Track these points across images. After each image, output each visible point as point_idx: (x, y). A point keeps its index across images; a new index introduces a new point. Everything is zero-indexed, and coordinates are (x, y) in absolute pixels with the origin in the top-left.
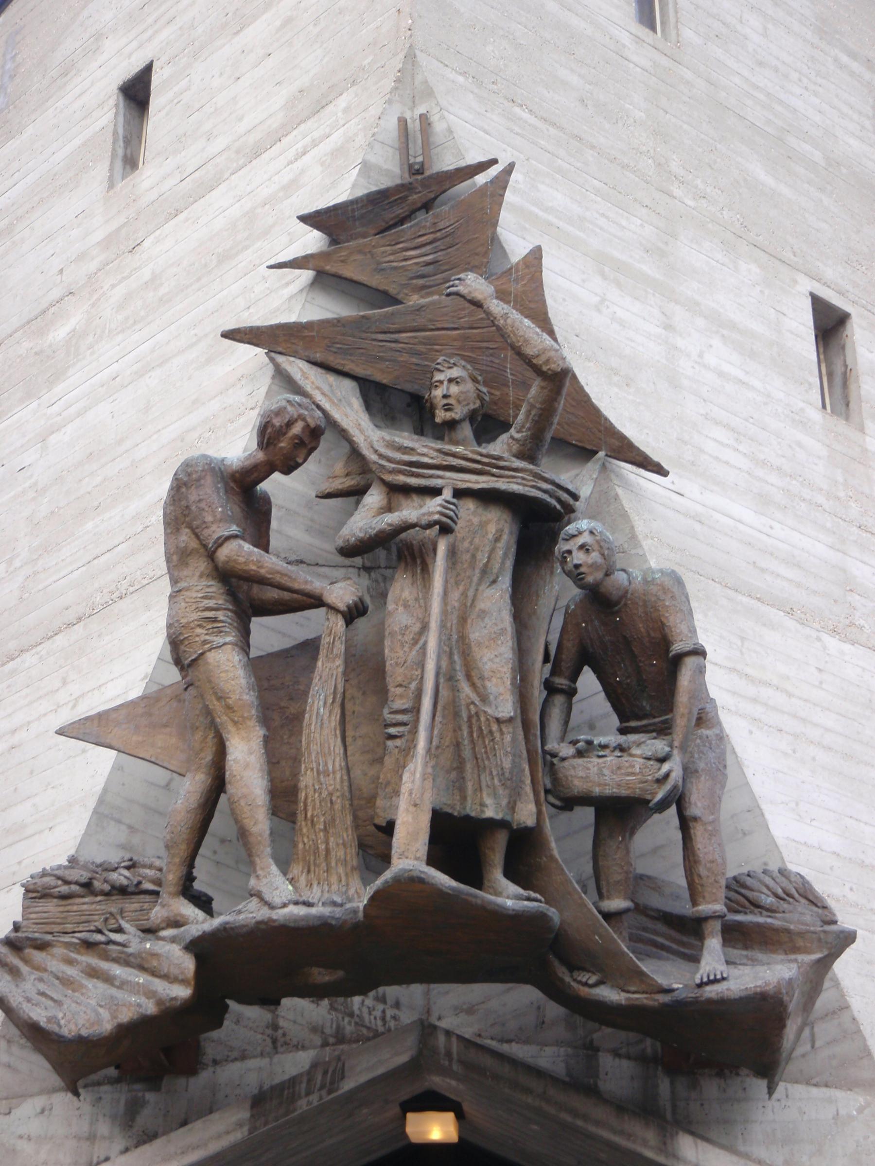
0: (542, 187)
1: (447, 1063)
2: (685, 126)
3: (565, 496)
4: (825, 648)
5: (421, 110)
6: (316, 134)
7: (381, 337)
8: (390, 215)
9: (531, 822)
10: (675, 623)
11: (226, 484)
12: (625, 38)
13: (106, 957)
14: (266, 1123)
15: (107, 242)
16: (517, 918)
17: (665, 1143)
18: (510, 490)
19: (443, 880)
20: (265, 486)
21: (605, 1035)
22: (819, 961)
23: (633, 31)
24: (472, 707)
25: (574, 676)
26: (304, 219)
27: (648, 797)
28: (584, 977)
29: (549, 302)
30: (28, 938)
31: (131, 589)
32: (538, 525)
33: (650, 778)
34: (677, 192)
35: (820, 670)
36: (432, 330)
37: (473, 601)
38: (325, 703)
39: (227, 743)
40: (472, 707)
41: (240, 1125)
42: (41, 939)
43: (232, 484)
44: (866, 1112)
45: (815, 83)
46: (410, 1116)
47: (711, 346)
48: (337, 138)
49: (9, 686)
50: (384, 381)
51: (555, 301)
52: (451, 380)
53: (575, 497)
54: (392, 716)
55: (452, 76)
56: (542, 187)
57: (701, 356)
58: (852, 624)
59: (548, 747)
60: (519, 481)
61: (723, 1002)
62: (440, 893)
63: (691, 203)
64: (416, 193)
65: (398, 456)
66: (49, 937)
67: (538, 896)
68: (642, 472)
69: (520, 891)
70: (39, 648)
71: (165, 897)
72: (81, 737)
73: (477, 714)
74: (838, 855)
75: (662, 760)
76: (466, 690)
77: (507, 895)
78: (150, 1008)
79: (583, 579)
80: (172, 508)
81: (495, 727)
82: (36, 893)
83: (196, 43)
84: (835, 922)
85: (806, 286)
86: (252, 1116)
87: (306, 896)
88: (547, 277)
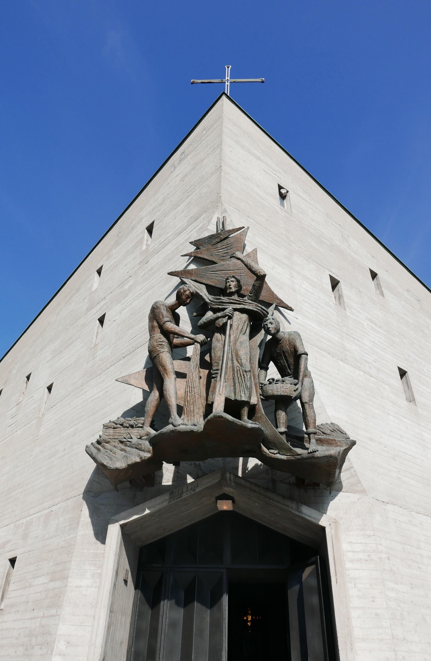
3: (264, 312)
6: (195, 226)
7: (212, 273)
10: (298, 344)
11: (167, 309)
12: (278, 208)
13: (126, 445)
14: (174, 500)
16: (253, 429)
17: (298, 508)
19: (229, 417)
22: (345, 449)
26: (191, 243)
27: (292, 395)
28: (272, 451)
30: (103, 440)
32: (257, 322)
38: (194, 368)
46: (219, 501)
52: (231, 281)
57: (301, 285)
58: (346, 359)
61: (318, 458)
62: (228, 420)
69: (252, 422)
71: (145, 427)
78: (138, 460)
81: (245, 373)
87: (187, 423)
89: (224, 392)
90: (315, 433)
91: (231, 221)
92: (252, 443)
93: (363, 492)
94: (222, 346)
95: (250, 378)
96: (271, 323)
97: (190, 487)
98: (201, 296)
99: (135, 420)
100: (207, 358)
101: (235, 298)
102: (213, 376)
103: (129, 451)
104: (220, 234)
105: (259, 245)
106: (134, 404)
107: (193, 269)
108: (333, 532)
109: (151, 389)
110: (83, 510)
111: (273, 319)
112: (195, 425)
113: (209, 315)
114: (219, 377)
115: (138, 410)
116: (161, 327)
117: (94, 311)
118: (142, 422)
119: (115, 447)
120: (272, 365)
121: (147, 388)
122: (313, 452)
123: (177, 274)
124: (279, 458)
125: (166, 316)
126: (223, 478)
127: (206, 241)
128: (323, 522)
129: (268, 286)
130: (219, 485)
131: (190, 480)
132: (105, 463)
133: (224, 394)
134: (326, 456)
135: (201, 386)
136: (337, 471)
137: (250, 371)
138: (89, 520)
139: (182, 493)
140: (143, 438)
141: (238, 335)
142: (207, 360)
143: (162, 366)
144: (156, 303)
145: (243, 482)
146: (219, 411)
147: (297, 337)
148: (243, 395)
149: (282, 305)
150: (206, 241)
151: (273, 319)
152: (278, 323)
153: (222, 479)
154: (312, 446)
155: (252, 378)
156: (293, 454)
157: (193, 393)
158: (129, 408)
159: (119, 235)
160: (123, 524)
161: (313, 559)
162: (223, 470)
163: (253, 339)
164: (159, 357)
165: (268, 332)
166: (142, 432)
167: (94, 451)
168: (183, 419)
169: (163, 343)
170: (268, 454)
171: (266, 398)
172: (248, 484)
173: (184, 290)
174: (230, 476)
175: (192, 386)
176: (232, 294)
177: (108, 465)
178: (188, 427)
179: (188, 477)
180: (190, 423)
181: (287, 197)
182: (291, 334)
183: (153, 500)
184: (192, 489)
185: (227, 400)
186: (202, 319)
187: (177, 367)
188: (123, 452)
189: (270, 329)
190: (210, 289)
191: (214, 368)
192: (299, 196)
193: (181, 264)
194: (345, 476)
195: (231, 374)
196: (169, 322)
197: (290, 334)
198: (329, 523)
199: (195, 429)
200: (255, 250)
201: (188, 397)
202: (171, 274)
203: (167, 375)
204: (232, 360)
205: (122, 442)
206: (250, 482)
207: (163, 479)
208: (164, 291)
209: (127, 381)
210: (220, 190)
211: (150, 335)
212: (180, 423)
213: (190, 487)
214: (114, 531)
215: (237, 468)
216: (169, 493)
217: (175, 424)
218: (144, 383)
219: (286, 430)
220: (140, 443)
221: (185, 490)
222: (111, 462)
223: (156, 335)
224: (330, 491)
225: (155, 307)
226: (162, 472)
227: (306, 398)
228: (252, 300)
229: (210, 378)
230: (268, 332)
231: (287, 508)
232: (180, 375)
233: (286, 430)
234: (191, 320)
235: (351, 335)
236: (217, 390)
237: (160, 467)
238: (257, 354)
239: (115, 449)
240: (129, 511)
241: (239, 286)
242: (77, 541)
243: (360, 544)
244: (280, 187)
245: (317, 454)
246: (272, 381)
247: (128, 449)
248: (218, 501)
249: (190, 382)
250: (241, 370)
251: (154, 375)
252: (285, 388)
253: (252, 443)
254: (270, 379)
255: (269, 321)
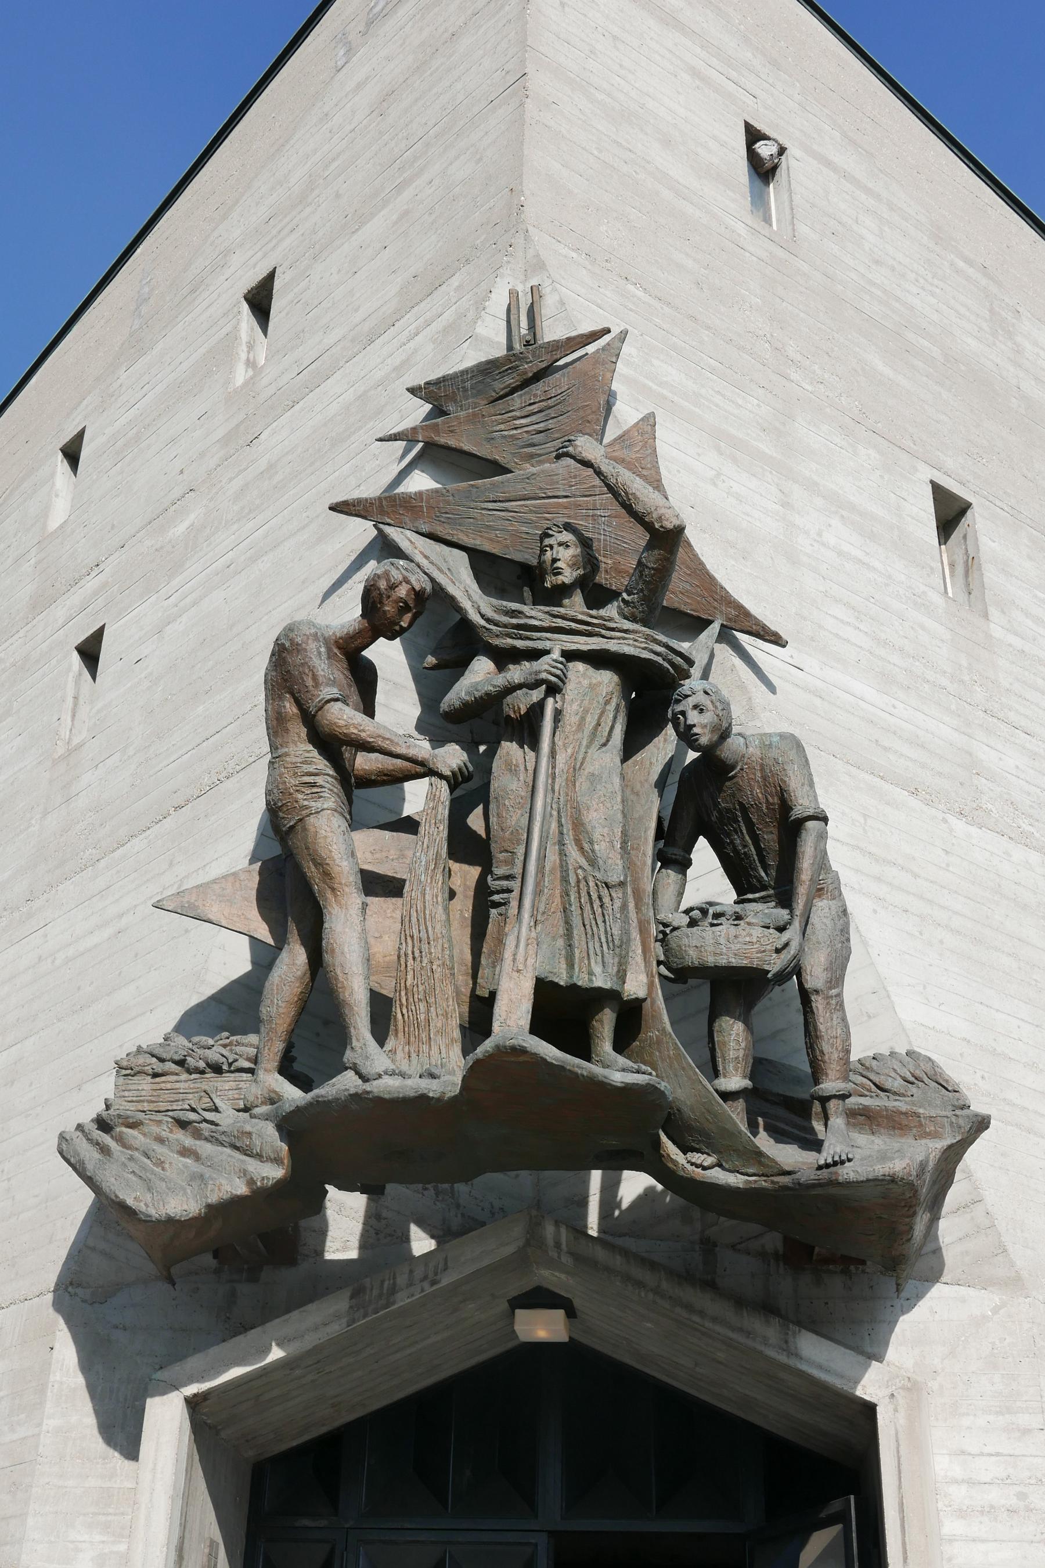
0: (656, 362)
1: (555, 1255)
2: (802, 315)
3: (678, 660)
4: (951, 830)
5: (534, 282)
7: (490, 505)
8: (500, 385)
9: (641, 994)
10: (794, 783)
11: (329, 650)
12: (741, 228)
13: (197, 1135)
14: (365, 1316)
15: (227, 440)
16: (628, 1090)
17: (786, 1342)
18: (622, 652)
19: (550, 1052)
20: (369, 653)
21: (725, 1227)
22: (950, 1147)
23: (749, 223)
24: (580, 871)
25: (689, 847)
26: (412, 391)
27: (766, 967)
29: (663, 471)
30: (119, 1116)
31: (238, 768)
32: (650, 696)
33: (768, 947)
34: (794, 376)
35: (947, 852)
36: (543, 498)
37: (582, 764)
38: (427, 869)
39: (325, 911)
40: (580, 871)
41: (337, 1316)
42: (132, 1117)
43: (336, 651)
44: (1002, 1312)
45: (932, 285)
46: (519, 1312)
47: (830, 526)
48: (448, 316)
49: (118, 872)
50: (494, 551)
51: (670, 472)
52: (560, 544)
53: (691, 663)
54: (497, 882)
55: (565, 251)
56: (656, 362)
57: (820, 534)
59: (661, 917)
60: (631, 642)
61: (848, 1184)
62: (541, 1062)
63: (809, 388)
64: (527, 363)
65: (505, 619)
66: (141, 1116)
67: (649, 1070)
68: (760, 643)
69: (629, 1063)
70: (148, 832)
71: (261, 1074)
72: (179, 911)
73: (585, 878)
74: (969, 1041)
75: (781, 929)
76: (574, 855)
77: (617, 1071)
78: (241, 1189)
79: (697, 740)
80: (274, 674)
81: (605, 892)
82: (126, 1070)
83: (317, 246)
84: (965, 1107)
85: (927, 474)
86: (351, 1307)
87: (404, 1067)
88: (662, 448)
89: (531, 961)
90: (843, 1097)
91: (562, 303)
92: (632, 1129)
93: (1015, 1283)
94: (524, 792)
95: (624, 907)
96: (699, 708)
97: (419, 1273)
98: (452, 599)
99: (225, 1046)
100: (475, 821)
101: (571, 613)
102: (496, 898)
103: (209, 1158)
104: (520, 357)
105: (665, 392)
106: (221, 983)
107: (420, 494)
108: (902, 1420)
109: (281, 940)
110: (57, 1346)
111: (706, 693)
112: (433, 1076)
113: (481, 674)
114: (514, 904)
115: (233, 1008)
116: (309, 719)
117: (59, 612)
118: (252, 1051)
119: (160, 1140)
120: (703, 852)
121: (264, 933)
122: (835, 1164)
123: (365, 509)
124: (720, 1182)
125: (328, 678)
126: (533, 1238)
127: (468, 384)
128: (870, 1387)
129: (696, 556)
130: (521, 1260)
131: (421, 1243)
132: (130, 1202)
133: (530, 969)
134: (875, 1180)
135: (455, 924)
136: (921, 1222)
137: (622, 884)
138: (80, 1380)
139: (393, 1290)
140: (256, 1111)
141: (583, 750)
142: (474, 828)
143: (317, 865)
144: (290, 629)
145: (600, 1254)
146: (515, 1030)
147: (792, 754)
148: (597, 969)
149: (746, 625)
150: (468, 384)
151: (706, 693)
152: (726, 706)
153: (528, 1243)
154: (838, 1137)
155: (631, 905)
156: (766, 1171)
157: (425, 961)
158: (203, 998)
159: (144, 309)
160: (195, 1395)
161: (836, 1506)
162: (534, 1213)
163: (638, 757)
164: (305, 829)
165: (687, 736)
166: (250, 1089)
167: (90, 1155)
168: (393, 1052)
169: (319, 780)
170: (684, 1168)
171: (679, 975)
172: (618, 1261)
173: (388, 580)
174: (558, 1233)
175: (423, 935)
176: (557, 595)
177: (140, 1207)
178: (409, 1082)
179: (415, 1231)
180: (413, 1067)
181: (781, 173)
182: (770, 746)
183: (295, 1315)
184: (425, 1278)
185: (544, 988)
186: (457, 686)
187: (368, 855)
188: (188, 1161)
189: (695, 730)
190: (488, 568)
191: (499, 871)
192: (829, 164)
193: (374, 471)
194: (949, 1229)
195: (558, 892)
196: (339, 704)
197: (766, 743)
198: (888, 1392)
199: (432, 1088)
200: (649, 421)
201: (410, 977)
202: (340, 508)
203: (336, 896)
204: (561, 843)
205: (183, 1124)
206: (626, 1253)
207: (329, 1238)
208: (315, 584)
209: (192, 906)
210: (521, 176)
211: (273, 747)
212: (380, 1069)
213: (419, 1273)
214: (166, 1418)
215: (583, 1203)
216: (347, 1293)
217: (364, 1071)
218: (254, 914)
219: (746, 1083)
220: (248, 1128)
221: (402, 1280)
222: (149, 1196)
223: (291, 749)
224: (898, 1285)
225: (287, 644)
226: (325, 1215)
227: (815, 976)
228: (633, 619)
229: (484, 902)
230: (687, 736)
231: (749, 1343)
232: (380, 885)
233: (746, 1083)
234: (417, 678)
235: (1001, 715)
236: (508, 955)
237: (316, 1204)
238: (650, 809)
239: (160, 1150)
240: (214, 1351)
241: (590, 561)
242: (41, 1449)
243: (993, 1459)
244: (753, 136)
245: (847, 1173)
246: (703, 915)
247: (206, 1148)
248: (517, 1311)
249: (414, 920)
250: (591, 879)
251: (289, 889)
252: (746, 940)
253: (632, 1129)
254: (692, 909)
255: (691, 701)
